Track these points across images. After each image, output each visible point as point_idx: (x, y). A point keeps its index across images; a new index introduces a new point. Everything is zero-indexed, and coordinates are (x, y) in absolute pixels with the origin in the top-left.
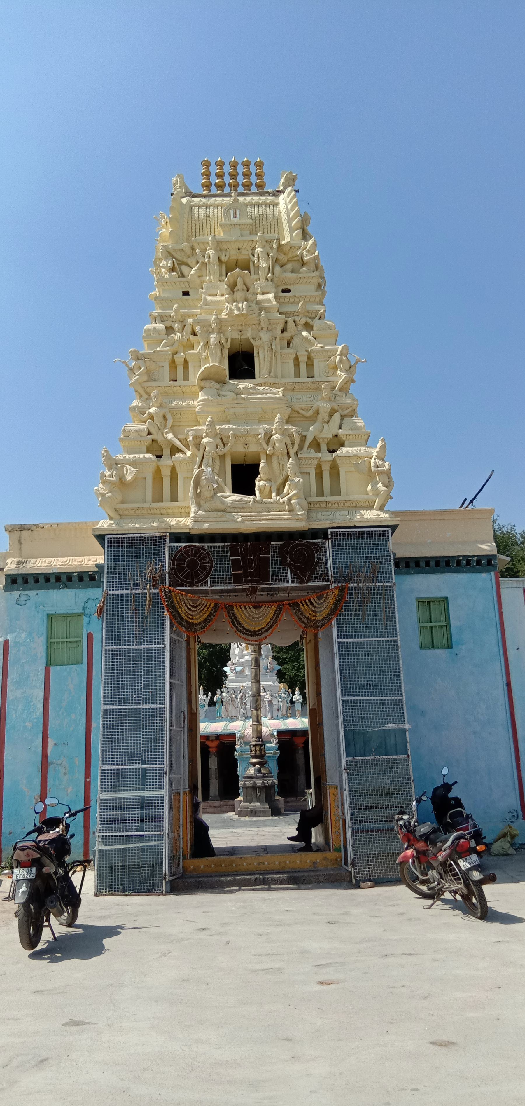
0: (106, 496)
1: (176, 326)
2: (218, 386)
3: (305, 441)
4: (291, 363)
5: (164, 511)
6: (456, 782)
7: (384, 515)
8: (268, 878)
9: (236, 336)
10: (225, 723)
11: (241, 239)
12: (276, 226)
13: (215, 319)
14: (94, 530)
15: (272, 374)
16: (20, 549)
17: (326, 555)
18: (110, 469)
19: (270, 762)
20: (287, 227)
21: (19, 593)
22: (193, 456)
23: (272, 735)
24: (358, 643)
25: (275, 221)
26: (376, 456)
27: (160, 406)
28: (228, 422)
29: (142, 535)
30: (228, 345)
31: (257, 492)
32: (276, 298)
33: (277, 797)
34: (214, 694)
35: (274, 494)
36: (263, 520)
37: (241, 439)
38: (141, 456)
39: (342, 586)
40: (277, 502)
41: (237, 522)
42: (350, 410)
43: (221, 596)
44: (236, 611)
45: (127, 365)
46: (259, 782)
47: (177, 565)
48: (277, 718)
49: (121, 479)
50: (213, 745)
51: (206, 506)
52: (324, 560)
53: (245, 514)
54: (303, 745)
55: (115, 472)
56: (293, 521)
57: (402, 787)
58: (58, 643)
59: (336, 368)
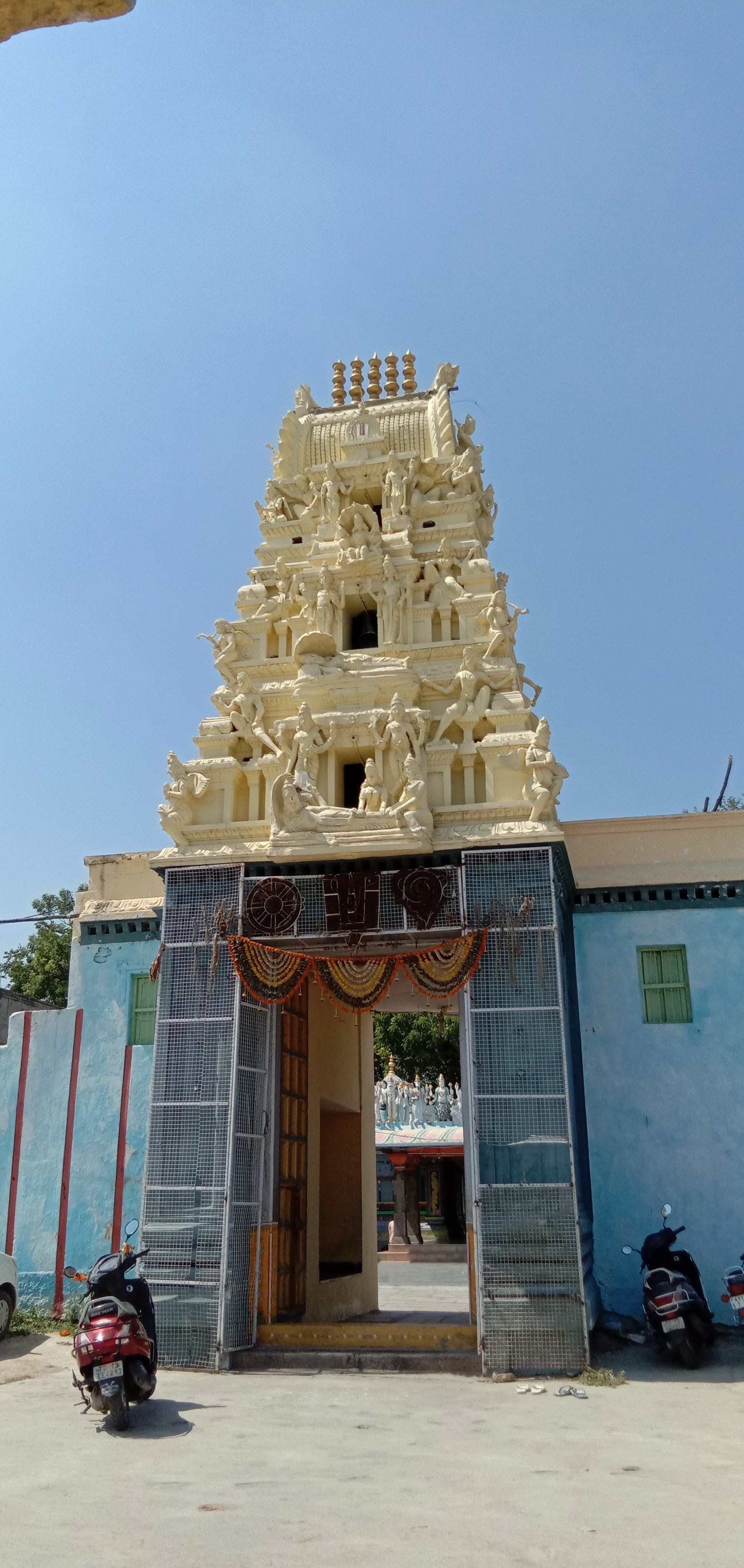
0: (169, 816)
1: (280, 583)
2: (321, 660)
3: (437, 727)
4: (428, 621)
5: (245, 833)
6: (682, 1229)
7: (541, 828)
9: (353, 591)
11: (368, 462)
12: (422, 440)
13: (324, 572)
14: (151, 863)
15: (399, 639)
16: (102, 888)
17: (457, 887)
18: (177, 779)
20: (435, 439)
21: (97, 946)
22: (285, 756)
24: (505, 1014)
25: (421, 433)
26: (535, 744)
27: (249, 693)
28: (334, 708)
29: (211, 867)
30: (342, 604)
31: (361, 803)
32: (411, 536)
35: (383, 804)
36: (366, 841)
37: (347, 730)
38: (218, 760)
39: (479, 931)
40: (386, 815)
41: (329, 845)
42: (505, 681)
43: (325, 948)
44: (331, 969)
45: (213, 641)
47: (253, 906)
49: (191, 791)
51: (291, 825)
52: (454, 895)
53: (341, 833)
55: (182, 783)
56: (406, 842)
57: (562, 1232)
58: (144, 1013)
59: (487, 626)
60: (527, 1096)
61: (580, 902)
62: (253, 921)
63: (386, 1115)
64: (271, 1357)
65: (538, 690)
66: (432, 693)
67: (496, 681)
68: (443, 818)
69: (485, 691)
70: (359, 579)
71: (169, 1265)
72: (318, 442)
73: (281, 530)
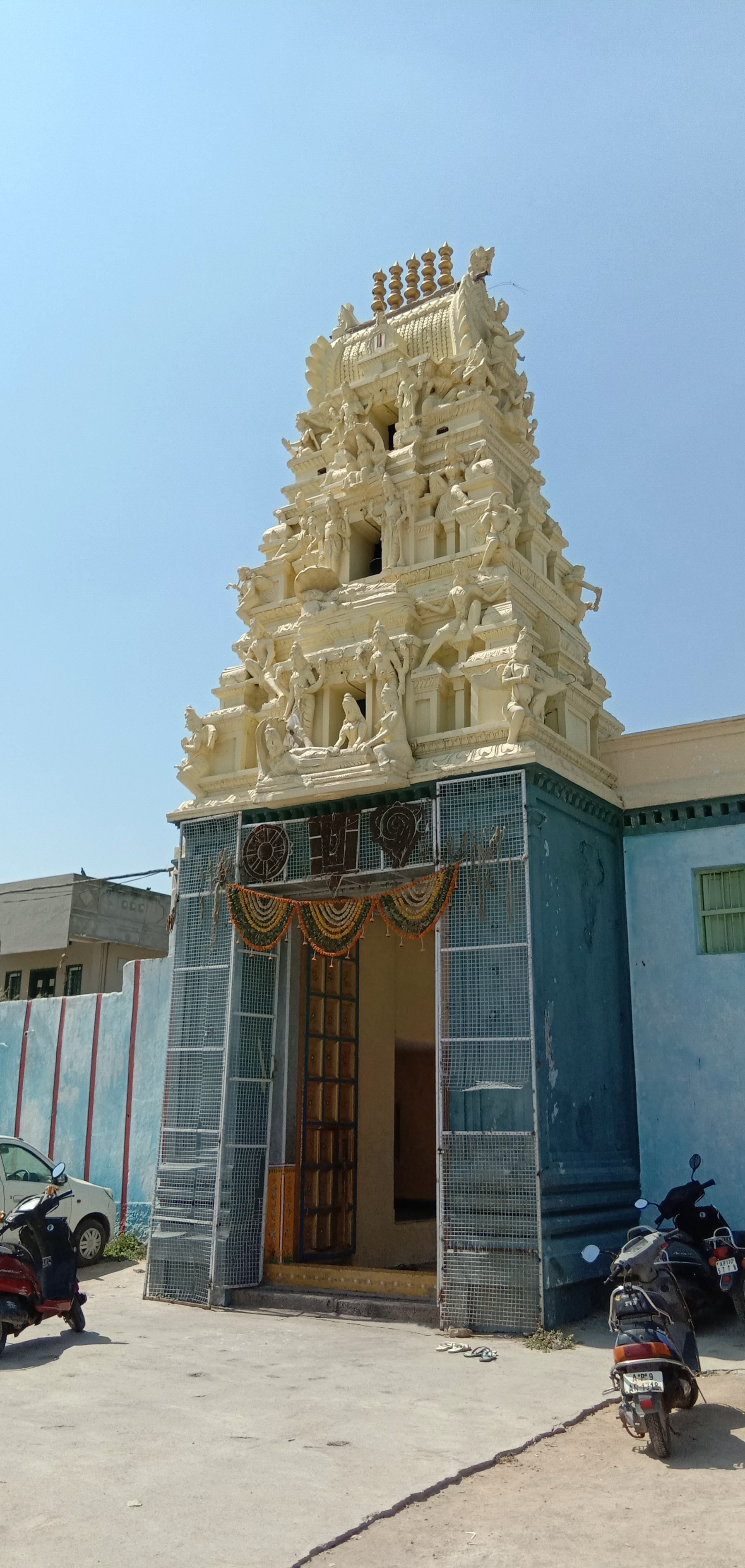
2: (320, 595)
6: (711, 1183)
8: (344, 1303)
9: (358, 517)
13: (328, 502)
15: (399, 562)
17: (431, 821)
36: (338, 780)
37: (337, 666)
42: (499, 591)
47: (249, 853)
52: (427, 829)
56: (373, 778)
60: (492, 1039)
61: (629, 824)
62: (248, 868)
64: (262, 1297)
65: (598, 592)
66: (432, 615)
67: (490, 593)
68: (426, 748)
69: (476, 606)
70: (364, 504)
71: (176, 1202)
72: (346, 363)
73: (306, 463)
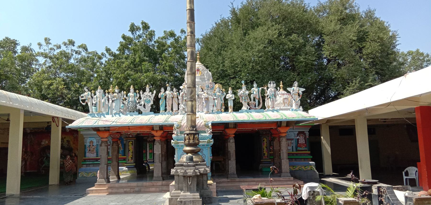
10: (167, 115)
19: (204, 149)
23: (206, 126)
33: (210, 182)
34: (159, 92)
46: (190, 172)
48: (213, 112)
50: (231, 132)
54: (234, 136)
63: (96, 110)
